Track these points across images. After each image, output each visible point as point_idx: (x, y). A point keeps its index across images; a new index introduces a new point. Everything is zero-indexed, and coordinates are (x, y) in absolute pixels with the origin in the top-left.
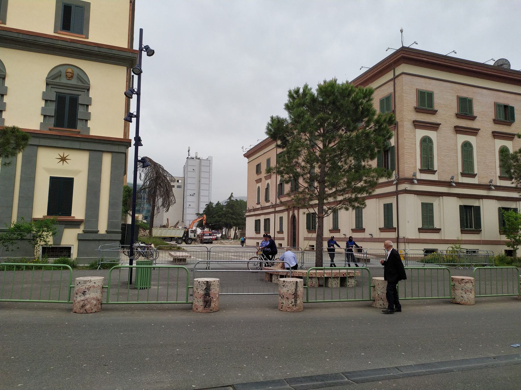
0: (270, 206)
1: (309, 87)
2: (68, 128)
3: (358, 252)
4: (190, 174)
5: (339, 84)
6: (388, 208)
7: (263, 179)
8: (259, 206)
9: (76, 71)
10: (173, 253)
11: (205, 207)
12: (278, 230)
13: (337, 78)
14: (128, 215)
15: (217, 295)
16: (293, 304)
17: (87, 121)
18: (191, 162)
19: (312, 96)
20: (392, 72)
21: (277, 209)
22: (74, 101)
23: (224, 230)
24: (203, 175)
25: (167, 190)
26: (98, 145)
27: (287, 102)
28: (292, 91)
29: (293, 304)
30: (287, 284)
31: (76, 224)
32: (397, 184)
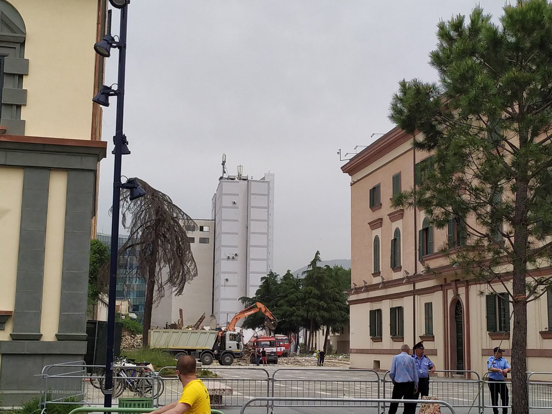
1: (485, 14)
4: (226, 214)
7: (386, 220)
8: (377, 280)
12: (423, 333)
17: (19, 107)
18: (228, 186)
21: (420, 286)
23: (301, 333)
25: (179, 247)
26: (41, 157)
27: (435, 48)
28: (447, 25)
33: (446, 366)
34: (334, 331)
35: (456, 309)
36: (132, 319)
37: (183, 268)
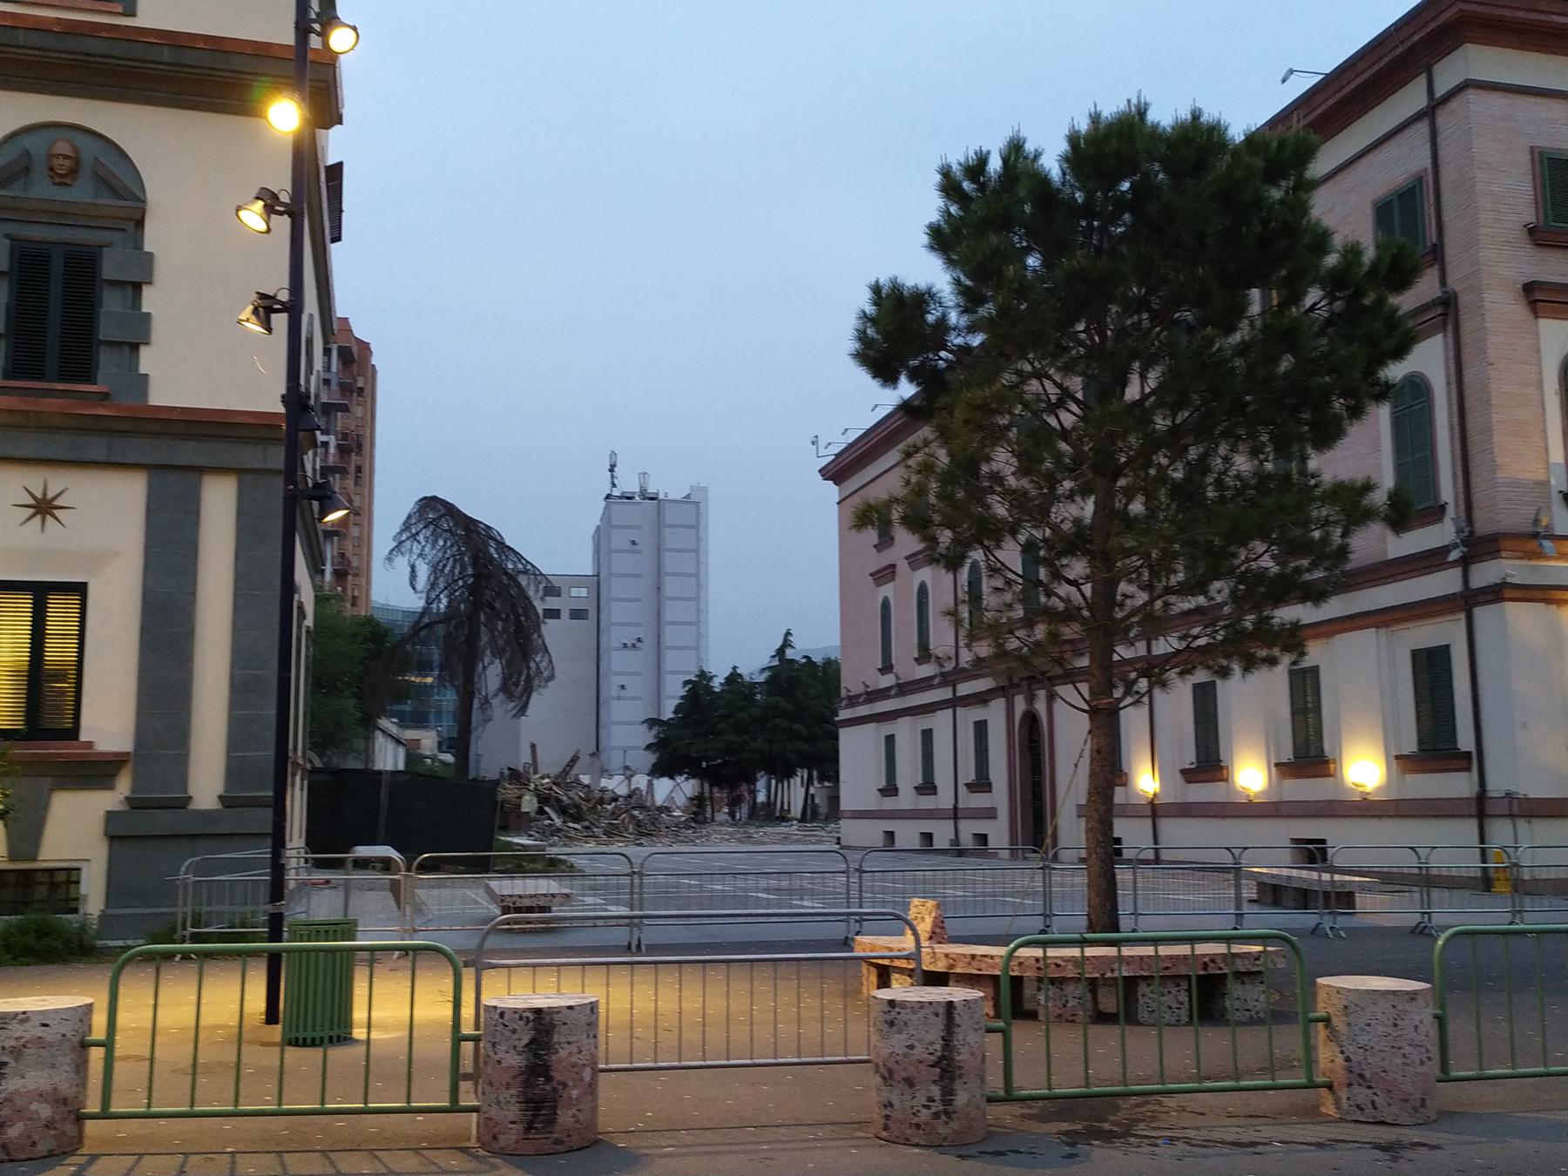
0: (932, 678)
1: (1030, 147)
2: (60, 380)
3: (1312, 859)
4: (621, 563)
5: (1155, 127)
6: (1431, 670)
7: (903, 567)
8: (887, 681)
9: (89, 149)
10: (494, 884)
11: (682, 692)
12: (972, 777)
13: (1148, 96)
14: (379, 734)
15: (587, 1074)
16: (937, 1106)
17: (135, 347)
18: (622, 512)
19: (1042, 180)
20: (1421, 81)
21: (965, 689)
22: (83, 269)
23: (761, 785)
24: (671, 562)
25: (519, 625)
26: (176, 449)
27: (934, 217)
28: (955, 167)
29: (937, 1106)
30: (905, 1015)
31: (95, 771)
32: (1465, 562)
33: (1013, 840)
34: (822, 779)
35: (1031, 732)
36: (443, 763)
37: (529, 667)
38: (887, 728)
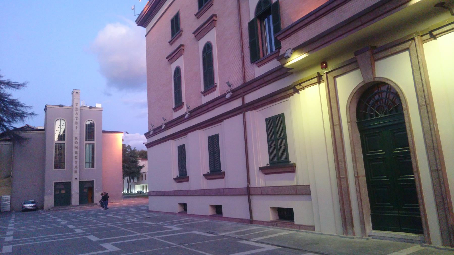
12: (264, 161)
38: (180, 141)
